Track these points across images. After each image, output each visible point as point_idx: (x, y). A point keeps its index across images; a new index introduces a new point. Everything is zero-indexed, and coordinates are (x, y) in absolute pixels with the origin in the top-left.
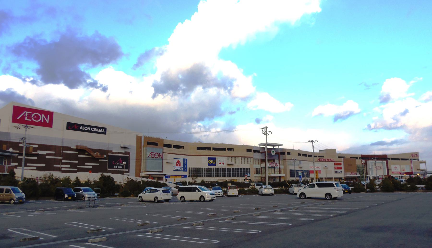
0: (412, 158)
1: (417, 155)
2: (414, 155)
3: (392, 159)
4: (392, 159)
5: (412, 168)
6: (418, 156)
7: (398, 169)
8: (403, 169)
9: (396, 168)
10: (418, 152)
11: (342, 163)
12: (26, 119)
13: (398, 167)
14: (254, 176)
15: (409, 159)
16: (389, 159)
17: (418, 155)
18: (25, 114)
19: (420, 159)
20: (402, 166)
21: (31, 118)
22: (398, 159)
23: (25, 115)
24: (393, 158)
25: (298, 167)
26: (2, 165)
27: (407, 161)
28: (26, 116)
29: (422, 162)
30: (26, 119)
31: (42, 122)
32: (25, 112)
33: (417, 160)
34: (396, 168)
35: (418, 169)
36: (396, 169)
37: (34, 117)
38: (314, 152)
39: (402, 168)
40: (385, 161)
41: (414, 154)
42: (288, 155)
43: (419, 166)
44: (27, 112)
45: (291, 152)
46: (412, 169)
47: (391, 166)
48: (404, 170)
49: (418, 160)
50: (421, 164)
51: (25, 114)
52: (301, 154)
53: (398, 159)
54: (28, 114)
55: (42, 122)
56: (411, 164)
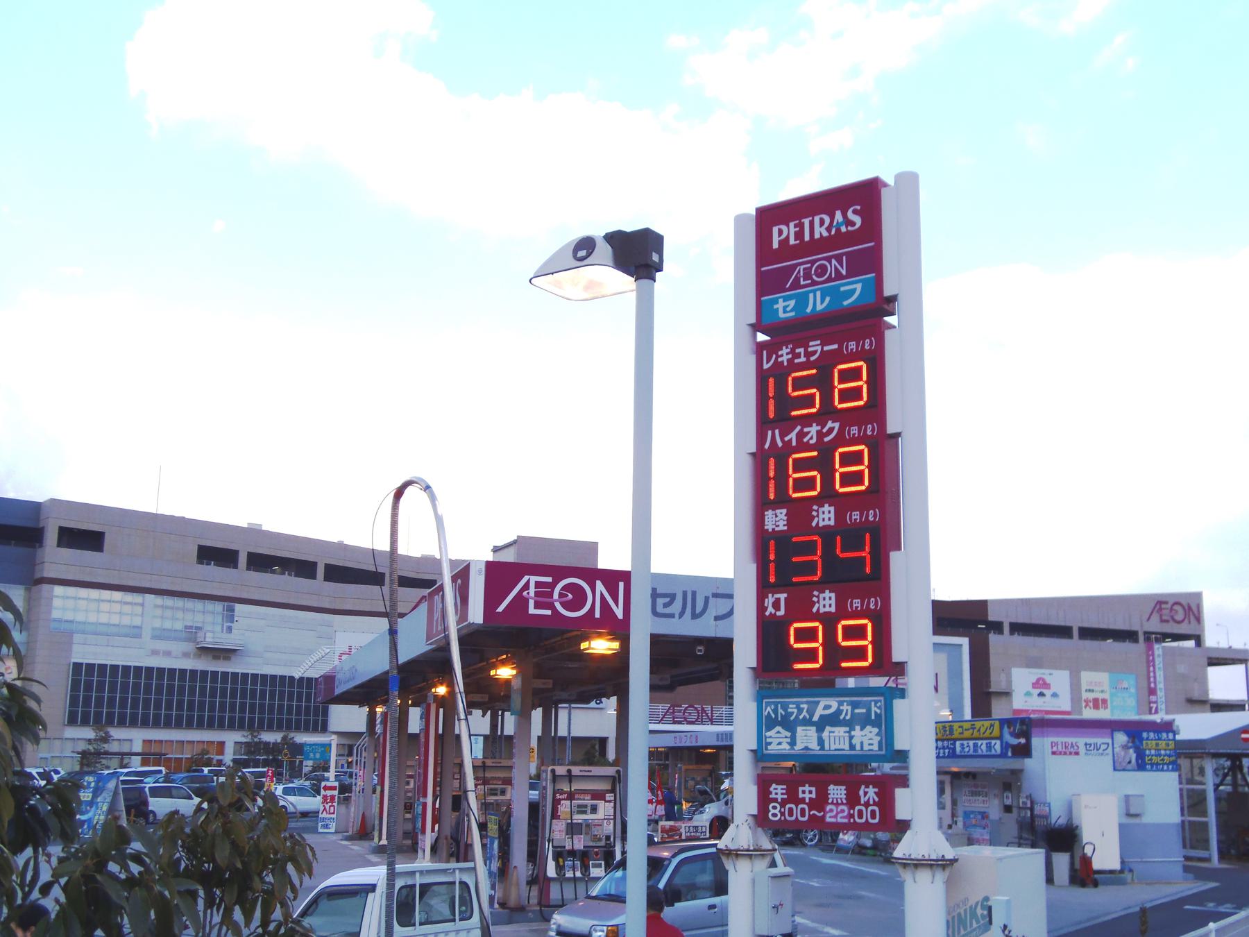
0: (1155, 625)
1: (1194, 608)
2: (1171, 609)
3: (1017, 628)
4: (1017, 628)
5: (1152, 692)
6: (1199, 619)
7: (1055, 695)
8: (1091, 696)
9: (1041, 684)
10: (1198, 596)
11: (1108, 711)
12: (532, 610)
13: (1059, 680)
14: (455, 764)
15: (1129, 636)
16: (997, 627)
17: (1199, 607)
18: (527, 586)
19: (1214, 639)
20: (1087, 677)
21: (551, 606)
22: (1063, 632)
23: (525, 593)
24: (1022, 619)
25: (189, 647)
26: (210, 768)
27: (1127, 646)
28: (532, 593)
29: (1220, 659)
30: (532, 610)
31: (597, 615)
32: (526, 578)
33: (1191, 644)
34: (1041, 684)
35: (1196, 695)
36: (1041, 694)
37: (561, 595)
38: (402, 550)
39: (1084, 687)
40: (964, 642)
41: (1171, 601)
42: (1054, 700)
43: (1203, 681)
44: (534, 579)
45: (58, 525)
46: (1153, 698)
47: (1009, 676)
48: (1096, 701)
49: (1198, 640)
50: (1214, 673)
51: (527, 586)
52: (314, 564)
53: (1063, 632)
54: (538, 584)
55: (597, 615)
56: (1150, 662)
